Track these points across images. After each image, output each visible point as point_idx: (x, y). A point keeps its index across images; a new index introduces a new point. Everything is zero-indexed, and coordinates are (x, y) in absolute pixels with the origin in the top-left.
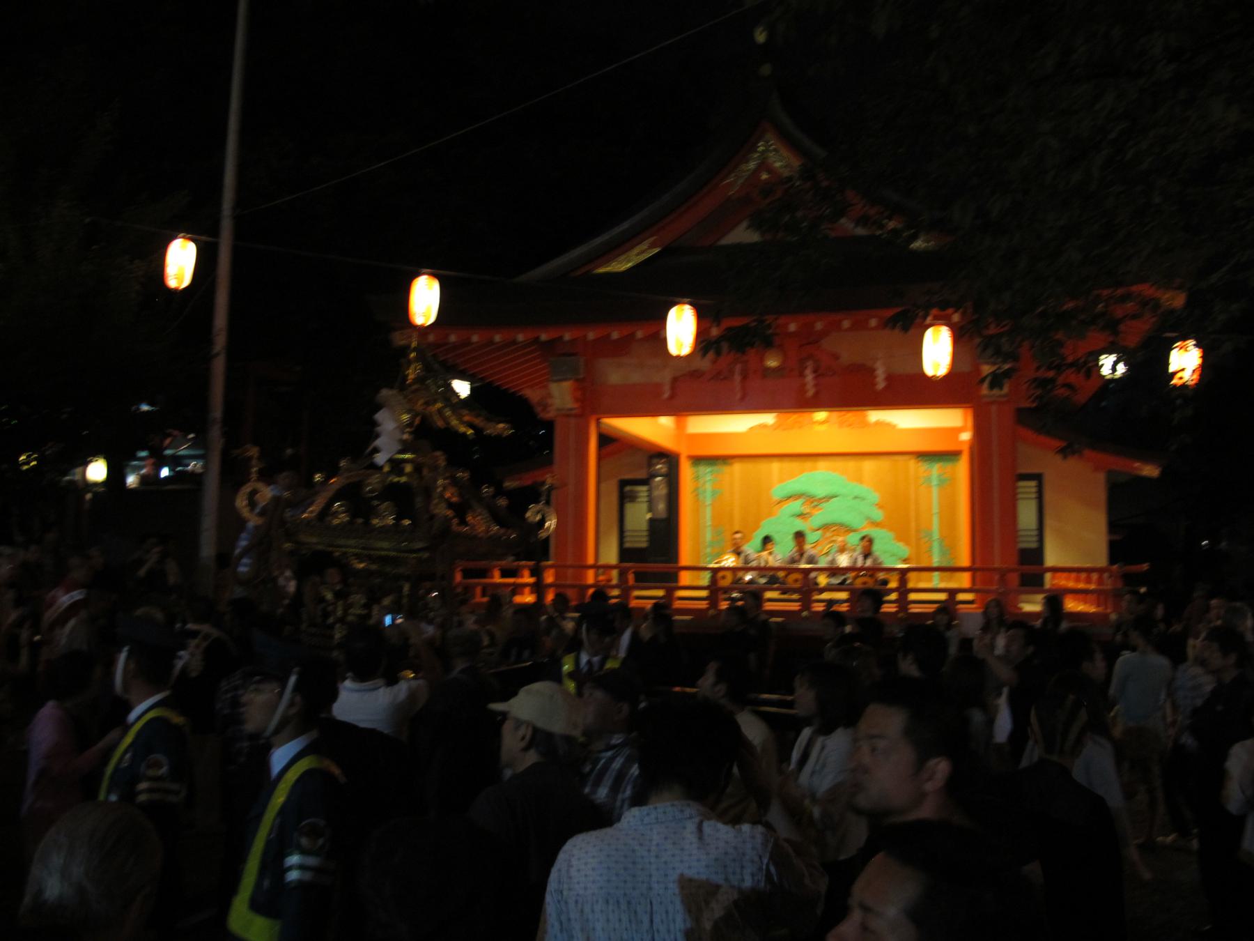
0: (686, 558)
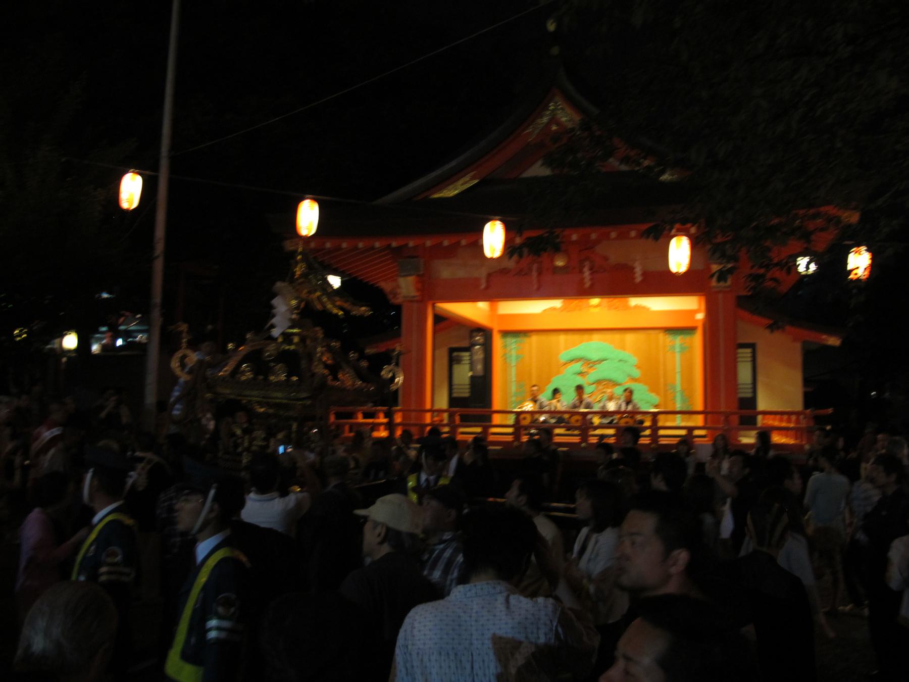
0: (497, 404)
